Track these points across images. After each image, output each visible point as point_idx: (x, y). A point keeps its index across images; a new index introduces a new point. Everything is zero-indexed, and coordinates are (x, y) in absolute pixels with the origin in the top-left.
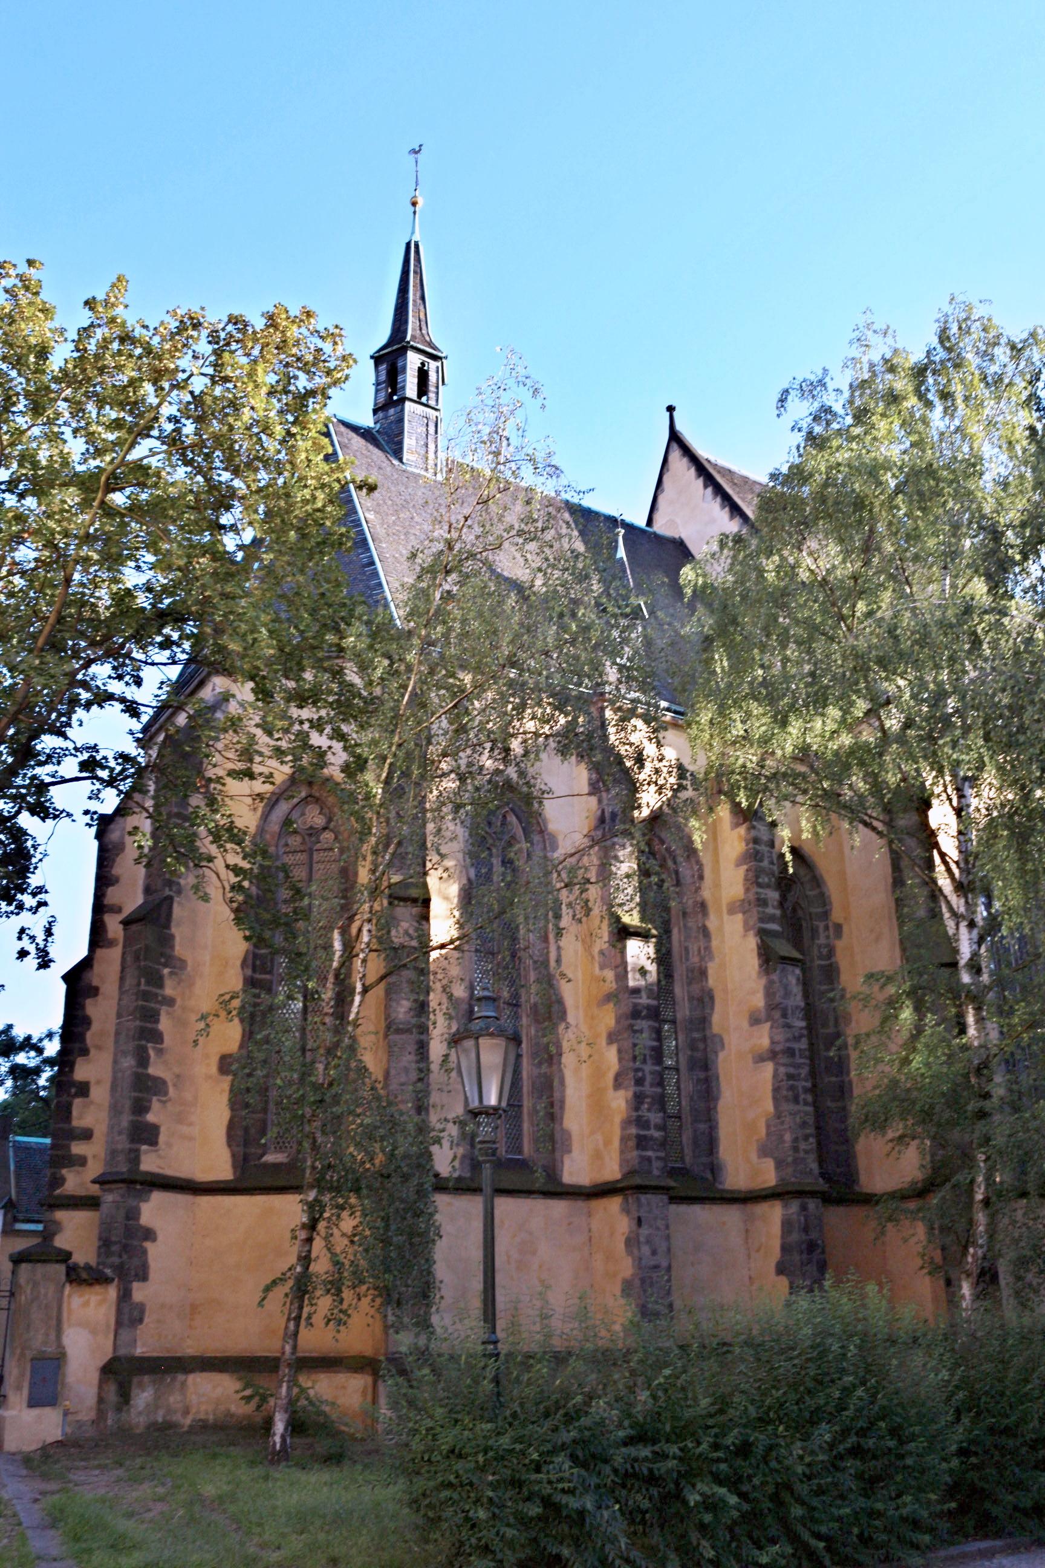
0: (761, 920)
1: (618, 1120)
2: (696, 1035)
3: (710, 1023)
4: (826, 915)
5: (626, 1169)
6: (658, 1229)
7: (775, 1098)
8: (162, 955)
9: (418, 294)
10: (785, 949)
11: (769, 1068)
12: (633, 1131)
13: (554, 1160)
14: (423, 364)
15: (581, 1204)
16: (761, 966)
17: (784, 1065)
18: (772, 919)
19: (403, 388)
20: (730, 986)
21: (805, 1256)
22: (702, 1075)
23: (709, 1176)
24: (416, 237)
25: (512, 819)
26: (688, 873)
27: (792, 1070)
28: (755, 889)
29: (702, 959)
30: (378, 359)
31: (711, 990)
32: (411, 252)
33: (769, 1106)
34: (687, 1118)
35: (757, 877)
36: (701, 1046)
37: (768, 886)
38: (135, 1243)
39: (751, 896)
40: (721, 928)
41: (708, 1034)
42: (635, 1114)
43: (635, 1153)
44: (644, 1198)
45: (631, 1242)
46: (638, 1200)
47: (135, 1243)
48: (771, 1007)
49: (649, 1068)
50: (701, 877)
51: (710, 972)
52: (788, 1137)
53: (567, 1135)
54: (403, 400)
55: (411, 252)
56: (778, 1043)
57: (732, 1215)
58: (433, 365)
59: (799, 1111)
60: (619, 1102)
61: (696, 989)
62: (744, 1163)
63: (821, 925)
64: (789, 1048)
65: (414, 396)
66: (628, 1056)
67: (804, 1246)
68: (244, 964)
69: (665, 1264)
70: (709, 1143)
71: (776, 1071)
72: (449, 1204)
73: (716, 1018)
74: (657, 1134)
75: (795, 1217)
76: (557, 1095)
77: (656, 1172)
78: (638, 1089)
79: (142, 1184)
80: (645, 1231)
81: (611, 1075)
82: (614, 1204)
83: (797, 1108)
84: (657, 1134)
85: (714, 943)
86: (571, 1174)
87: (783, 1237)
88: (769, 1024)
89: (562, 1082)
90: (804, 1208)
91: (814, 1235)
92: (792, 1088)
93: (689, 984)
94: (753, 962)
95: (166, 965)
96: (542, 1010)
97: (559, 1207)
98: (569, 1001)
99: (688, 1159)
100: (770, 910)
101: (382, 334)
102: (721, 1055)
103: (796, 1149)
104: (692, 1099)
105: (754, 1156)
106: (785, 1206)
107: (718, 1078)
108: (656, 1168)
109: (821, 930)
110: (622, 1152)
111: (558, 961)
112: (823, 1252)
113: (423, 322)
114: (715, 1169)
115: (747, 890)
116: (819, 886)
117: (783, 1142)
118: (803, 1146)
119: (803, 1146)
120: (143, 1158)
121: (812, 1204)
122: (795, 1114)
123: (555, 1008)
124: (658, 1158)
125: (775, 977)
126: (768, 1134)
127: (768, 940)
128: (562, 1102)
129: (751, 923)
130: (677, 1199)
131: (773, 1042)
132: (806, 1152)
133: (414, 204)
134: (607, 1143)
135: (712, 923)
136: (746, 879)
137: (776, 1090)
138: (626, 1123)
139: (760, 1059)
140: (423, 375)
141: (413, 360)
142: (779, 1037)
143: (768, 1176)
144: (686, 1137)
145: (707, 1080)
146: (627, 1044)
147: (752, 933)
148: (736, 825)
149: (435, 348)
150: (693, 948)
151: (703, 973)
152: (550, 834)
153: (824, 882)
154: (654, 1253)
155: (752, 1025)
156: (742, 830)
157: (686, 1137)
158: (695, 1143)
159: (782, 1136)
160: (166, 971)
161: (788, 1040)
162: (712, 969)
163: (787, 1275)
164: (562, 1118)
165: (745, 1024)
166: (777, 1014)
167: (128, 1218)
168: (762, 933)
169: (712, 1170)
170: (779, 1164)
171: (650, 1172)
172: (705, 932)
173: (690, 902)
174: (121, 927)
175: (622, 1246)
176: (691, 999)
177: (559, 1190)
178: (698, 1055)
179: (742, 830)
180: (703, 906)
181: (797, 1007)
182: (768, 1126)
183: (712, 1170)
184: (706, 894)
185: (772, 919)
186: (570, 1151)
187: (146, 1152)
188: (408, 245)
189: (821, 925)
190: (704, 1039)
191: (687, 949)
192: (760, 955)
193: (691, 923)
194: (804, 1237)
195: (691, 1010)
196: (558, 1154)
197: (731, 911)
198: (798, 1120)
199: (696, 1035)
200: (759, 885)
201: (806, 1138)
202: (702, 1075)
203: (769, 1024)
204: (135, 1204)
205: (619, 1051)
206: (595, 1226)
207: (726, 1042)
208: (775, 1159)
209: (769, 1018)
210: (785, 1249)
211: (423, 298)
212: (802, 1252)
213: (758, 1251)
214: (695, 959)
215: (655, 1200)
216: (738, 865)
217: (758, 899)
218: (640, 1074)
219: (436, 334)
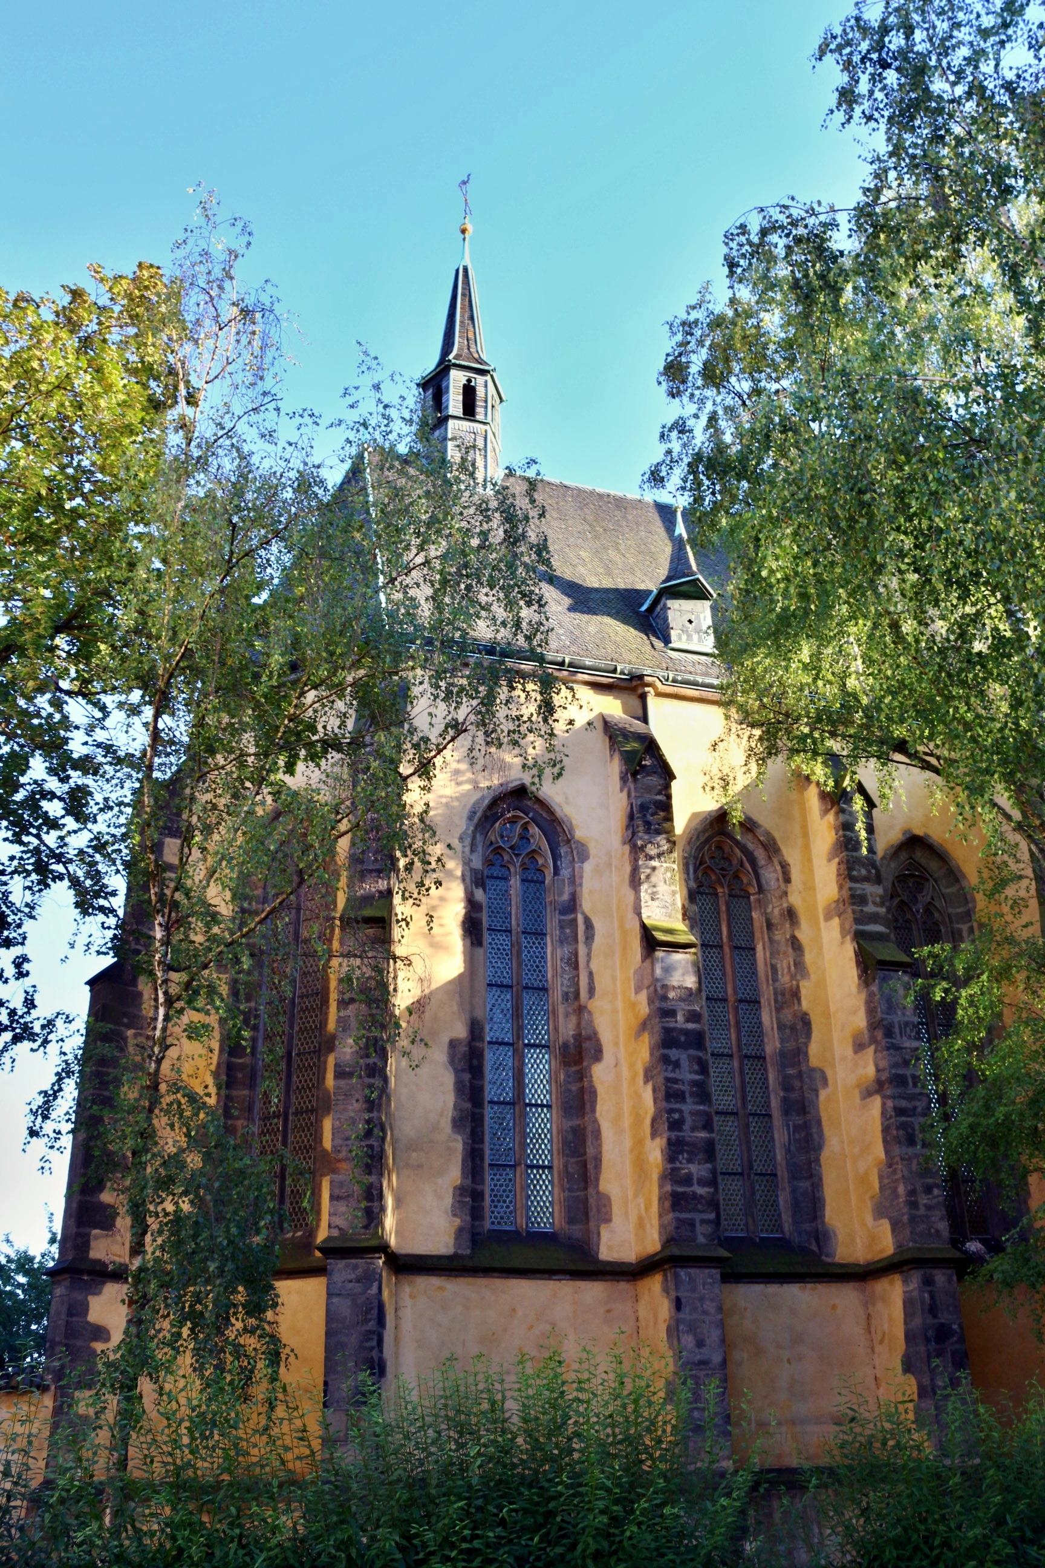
0: (857, 921)
1: (655, 1177)
2: (791, 1071)
3: (806, 1054)
4: (968, 915)
5: (664, 1238)
6: (705, 1312)
7: (885, 1142)
8: (125, 1014)
9: (466, 316)
10: (890, 952)
11: (877, 1102)
12: (668, 1188)
13: (588, 1231)
14: (469, 381)
15: (623, 1286)
16: (860, 977)
17: (893, 1097)
18: (873, 918)
19: (447, 407)
20: (832, 1008)
21: (933, 1345)
22: (799, 1120)
23: (814, 1247)
24: (467, 261)
25: (534, 830)
26: (773, 876)
27: (903, 1104)
28: (849, 884)
29: (793, 977)
30: (424, 385)
31: (806, 1014)
32: (462, 281)
33: (879, 1151)
34: (782, 1173)
35: (850, 869)
36: (797, 1084)
37: (866, 879)
38: (79, 1343)
39: (846, 893)
40: (817, 940)
41: (804, 1069)
42: (669, 1166)
43: (671, 1216)
44: (683, 1273)
45: (673, 1331)
46: (676, 1276)
47: (79, 1343)
48: (873, 1026)
49: (689, 1107)
50: (787, 880)
51: (803, 992)
52: (901, 1190)
53: (605, 1201)
54: (447, 418)
55: (462, 281)
56: (884, 1070)
57: (845, 1298)
58: (479, 381)
59: (916, 1156)
60: (655, 1152)
61: (787, 1015)
62: (858, 1226)
63: (965, 928)
64: (897, 1076)
65: (459, 412)
66: (661, 1095)
67: (930, 1333)
68: (594, 1093)
69: (717, 1359)
70: (811, 1204)
71: (884, 1105)
72: (441, 1288)
73: (814, 1049)
74: (701, 1191)
75: (916, 1294)
76: (590, 1151)
77: (701, 1239)
78: (674, 1135)
79: (90, 1273)
80: (685, 1315)
81: (648, 1121)
82: (655, 1284)
83: (910, 1151)
84: (701, 1191)
85: (808, 957)
86: (610, 1248)
87: (906, 1323)
88: (873, 1047)
89: (597, 1134)
90: (928, 1282)
91: (945, 1318)
92: (903, 1126)
93: (778, 1010)
94: (852, 972)
95: (129, 1026)
96: (572, 1050)
97: (593, 1291)
98: (606, 1037)
99: (787, 1227)
100: (870, 908)
101: (429, 363)
102: (823, 1094)
103: (913, 1205)
104: (788, 1151)
105: (869, 1219)
106: (905, 1282)
107: (819, 1122)
108: (702, 1233)
109: (965, 934)
110: (660, 1216)
111: (591, 991)
112: (962, 1339)
113: (470, 341)
114: (822, 1236)
115: (841, 887)
116: (957, 880)
117: (897, 1196)
118: (923, 1200)
119: (923, 1200)
120: (93, 1244)
121: (940, 1277)
122: (910, 1159)
123: (586, 1045)
124: (703, 1221)
125: (874, 988)
126: (881, 1188)
127: (868, 946)
128: (598, 1160)
129: (847, 927)
130: (732, 1276)
131: (878, 1070)
132: (928, 1207)
133: (463, 231)
134: (647, 1208)
135: (804, 934)
136: (839, 875)
137: (885, 1130)
138: (663, 1178)
139: (868, 1094)
140: (469, 392)
141: (457, 379)
142: (884, 1064)
143: (886, 1243)
144: (784, 1199)
145: (806, 1126)
146: (660, 1080)
147: (848, 938)
148: (825, 812)
149: (480, 361)
150: (784, 964)
151: (796, 994)
152: (578, 842)
153: (964, 876)
154: (700, 1344)
155: (856, 1052)
156: (831, 817)
157: (784, 1199)
158: (796, 1205)
159: (895, 1189)
160: (130, 1033)
161: (895, 1065)
162: (806, 989)
163: (913, 1374)
164: (597, 1179)
165: (849, 1051)
166: (879, 1034)
167: (70, 1314)
168: (860, 937)
169: (817, 1239)
170: (895, 1226)
171: (694, 1240)
172: (796, 945)
173: (776, 911)
174: (88, 988)
175: (664, 1335)
176: (781, 1027)
177: (592, 1268)
178: (794, 1096)
179: (831, 817)
180: (791, 915)
181: (907, 1024)
182: (881, 1177)
183: (817, 1239)
184: (795, 899)
185: (873, 918)
186: (608, 1220)
187: (97, 1238)
188: (457, 271)
189: (965, 928)
190: (800, 1074)
191: (774, 968)
192: (858, 963)
193: (778, 936)
194: (930, 1320)
195: (782, 1041)
196: (592, 1224)
197: (828, 917)
198: (914, 1167)
199: (791, 1071)
200: (852, 879)
201: (928, 1190)
202: (799, 1120)
203: (873, 1047)
204: (80, 1297)
205: (654, 1091)
206: (642, 1314)
207: (829, 1073)
208: (890, 1219)
209: (873, 1040)
210: (909, 1337)
211: (472, 318)
212: (928, 1341)
213: (881, 1342)
214: (784, 979)
215: (705, 1278)
216: (829, 860)
217: (852, 896)
218: (676, 1116)
219: (488, 352)
